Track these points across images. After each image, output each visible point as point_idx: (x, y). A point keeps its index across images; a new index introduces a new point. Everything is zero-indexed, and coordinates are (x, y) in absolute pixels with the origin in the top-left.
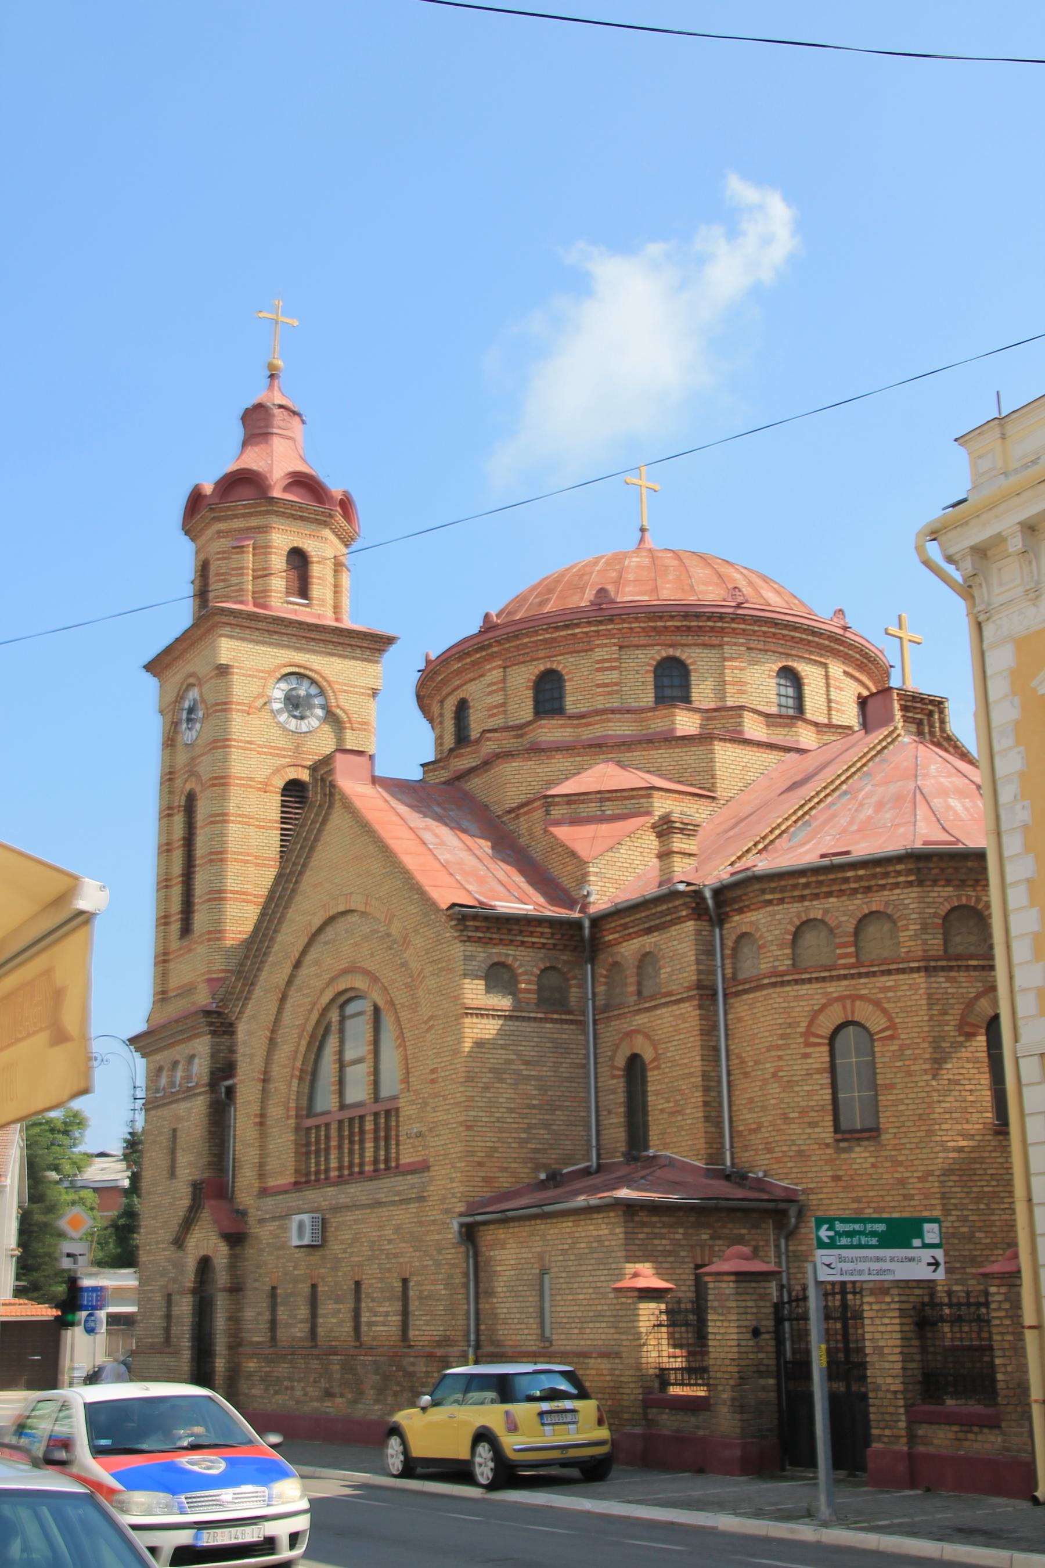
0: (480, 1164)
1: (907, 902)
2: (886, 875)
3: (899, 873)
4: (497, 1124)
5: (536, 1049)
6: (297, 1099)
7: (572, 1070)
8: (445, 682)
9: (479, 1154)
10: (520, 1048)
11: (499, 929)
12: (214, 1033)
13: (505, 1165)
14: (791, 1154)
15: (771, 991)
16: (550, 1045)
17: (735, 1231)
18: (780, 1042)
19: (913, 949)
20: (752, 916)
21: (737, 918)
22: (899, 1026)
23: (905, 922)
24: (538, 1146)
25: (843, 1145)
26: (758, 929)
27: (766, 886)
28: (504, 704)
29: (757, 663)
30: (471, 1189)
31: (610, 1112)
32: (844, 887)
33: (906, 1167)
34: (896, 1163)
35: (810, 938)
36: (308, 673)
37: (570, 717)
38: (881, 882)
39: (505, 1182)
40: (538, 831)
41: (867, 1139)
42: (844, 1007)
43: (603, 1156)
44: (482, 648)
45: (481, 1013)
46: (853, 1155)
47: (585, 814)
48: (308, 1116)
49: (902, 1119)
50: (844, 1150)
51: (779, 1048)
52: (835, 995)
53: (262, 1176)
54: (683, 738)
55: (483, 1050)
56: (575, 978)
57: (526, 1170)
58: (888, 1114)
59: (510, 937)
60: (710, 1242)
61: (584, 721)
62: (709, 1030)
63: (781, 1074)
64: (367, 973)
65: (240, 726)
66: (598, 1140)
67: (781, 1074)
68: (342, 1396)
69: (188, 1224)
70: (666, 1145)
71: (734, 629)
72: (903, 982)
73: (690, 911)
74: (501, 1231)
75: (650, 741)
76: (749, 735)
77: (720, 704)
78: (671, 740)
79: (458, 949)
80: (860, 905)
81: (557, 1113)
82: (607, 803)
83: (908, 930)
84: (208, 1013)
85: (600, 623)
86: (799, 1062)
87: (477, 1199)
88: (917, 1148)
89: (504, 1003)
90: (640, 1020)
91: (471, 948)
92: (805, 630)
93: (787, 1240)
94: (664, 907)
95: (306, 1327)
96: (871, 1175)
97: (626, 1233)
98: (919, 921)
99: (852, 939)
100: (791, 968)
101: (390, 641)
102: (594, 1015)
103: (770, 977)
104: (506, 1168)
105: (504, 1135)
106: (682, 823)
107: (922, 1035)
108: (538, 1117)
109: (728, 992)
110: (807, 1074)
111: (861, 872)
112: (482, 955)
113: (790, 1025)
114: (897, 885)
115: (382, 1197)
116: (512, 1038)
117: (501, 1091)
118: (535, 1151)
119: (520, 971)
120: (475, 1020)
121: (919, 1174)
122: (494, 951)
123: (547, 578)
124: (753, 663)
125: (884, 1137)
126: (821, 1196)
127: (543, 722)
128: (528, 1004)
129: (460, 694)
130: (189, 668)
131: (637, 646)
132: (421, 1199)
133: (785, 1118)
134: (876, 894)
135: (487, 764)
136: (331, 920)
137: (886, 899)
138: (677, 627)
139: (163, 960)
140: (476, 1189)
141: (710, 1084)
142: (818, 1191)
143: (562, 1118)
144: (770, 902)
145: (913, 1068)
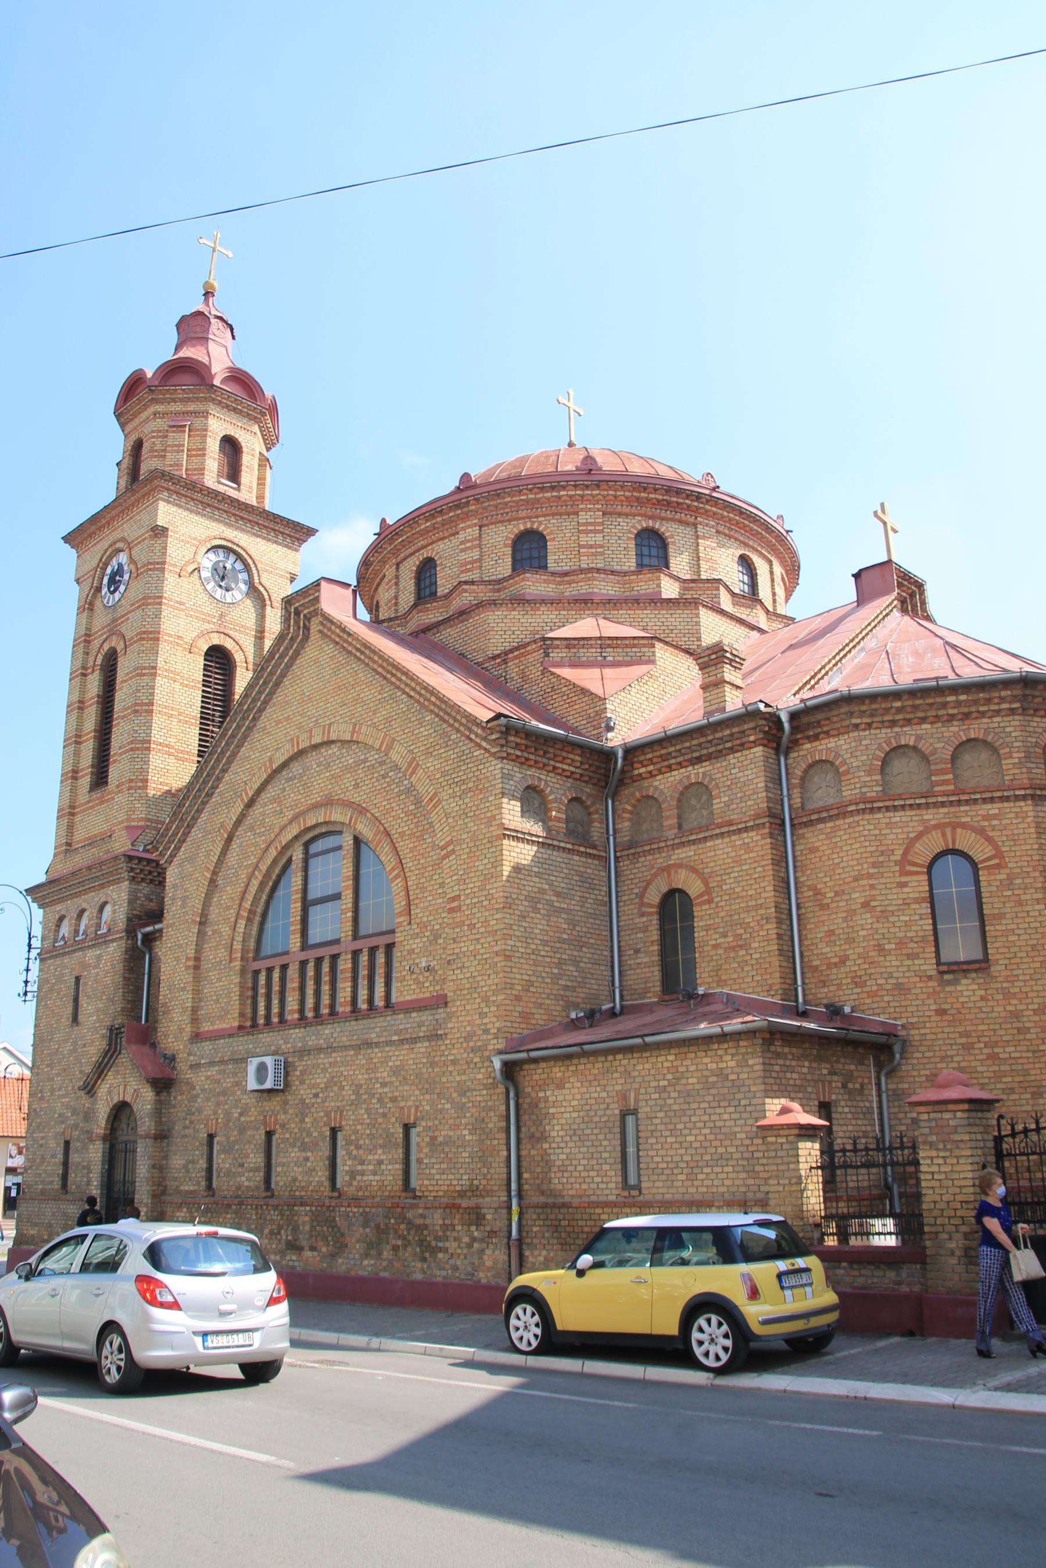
0: (518, 998)
1: (1008, 730)
2: (989, 701)
3: (1002, 700)
4: (532, 957)
5: (565, 881)
6: (244, 941)
7: (595, 907)
8: (410, 542)
9: (517, 987)
10: (552, 878)
11: (536, 749)
12: (133, 879)
13: (539, 1001)
14: (888, 987)
15: (857, 818)
16: (577, 878)
17: (847, 1067)
18: (872, 871)
19: (1017, 777)
20: (831, 743)
21: (808, 746)
22: (1005, 854)
23: (1008, 750)
24: (569, 984)
25: (946, 977)
26: (838, 755)
27: (855, 708)
28: (480, 560)
29: (723, 546)
30: (509, 1024)
31: (637, 951)
32: (941, 713)
33: (1020, 1000)
34: (1008, 995)
35: (900, 766)
36: (235, 547)
37: (553, 574)
38: (982, 709)
39: (540, 1019)
40: (535, 672)
41: (976, 971)
42: (944, 835)
43: (626, 998)
44: (458, 507)
45: (519, 837)
46: (959, 988)
47: (585, 659)
48: (255, 959)
49: (1013, 950)
50: (949, 983)
51: (870, 876)
52: (933, 822)
53: (195, 1020)
54: (669, 600)
55: (519, 876)
56: (597, 812)
57: (558, 1008)
58: (997, 945)
59: (545, 760)
60: (828, 1078)
61: (566, 579)
62: (780, 860)
63: (873, 904)
64: (348, 804)
65: (173, 586)
66: (620, 981)
67: (873, 904)
68: (313, 1249)
69: (101, 1070)
70: (721, 983)
71: (707, 511)
72: (1008, 810)
73: (761, 735)
74: (557, 1069)
75: (637, 601)
76: (723, 606)
77: (696, 577)
78: (657, 601)
79: (496, 768)
80: (956, 732)
81: (585, 950)
82: (608, 650)
83: (1011, 757)
84: (130, 858)
85: (587, 487)
86: (894, 891)
87: (515, 1036)
88: (1031, 979)
89: (537, 829)
90: (682, 854)
91: (508, 766)
92: (763, 524)
93: (887, 1078)
94: (727, 732)
95: (260, 1176)
96: (980, 1008)
97: (764, 1064)
98: (1022, 749)
99: (949, 766)
100: (881, 794)
101: (311, 532)
102: (615, 852)
103: (857, 804)
104: (541, 1004)
105: (539, 969)
106: (732, 654)
107: (1031, 864)
108: (569, 952)
109: (796, 822)
110: (904, 904)
111: (963, 697)
112: (521, 776)
113: (882, 853)
114: (997, 712)
115: (373, 1036)
116: (545, 866)
117: (535, 921)
118: (566, 988)
119: (551, 798)
120: (513, 843)
121: (1036, 1007)
122: (528, 773)
123: (499, 466)
124: (721, 545)
125: (993, 969)
126: (922, 1031)
127: (528, 575)
128: (558, 832)
129: (425, 554)
130: (117, 534)
131: (620, 514)
132: (434, 1037)
133: (880, 949)
134: (973, 722)
135: (463, 614)
136: (301, 753)
137: (986, 726)
138: (659, 501)
139: (69, 813)
140: (515, 1025)
141: (783, 917)
142: (920, 1026)
143: (588, 955)
144: (856, 726)
145: (1023, 897)
